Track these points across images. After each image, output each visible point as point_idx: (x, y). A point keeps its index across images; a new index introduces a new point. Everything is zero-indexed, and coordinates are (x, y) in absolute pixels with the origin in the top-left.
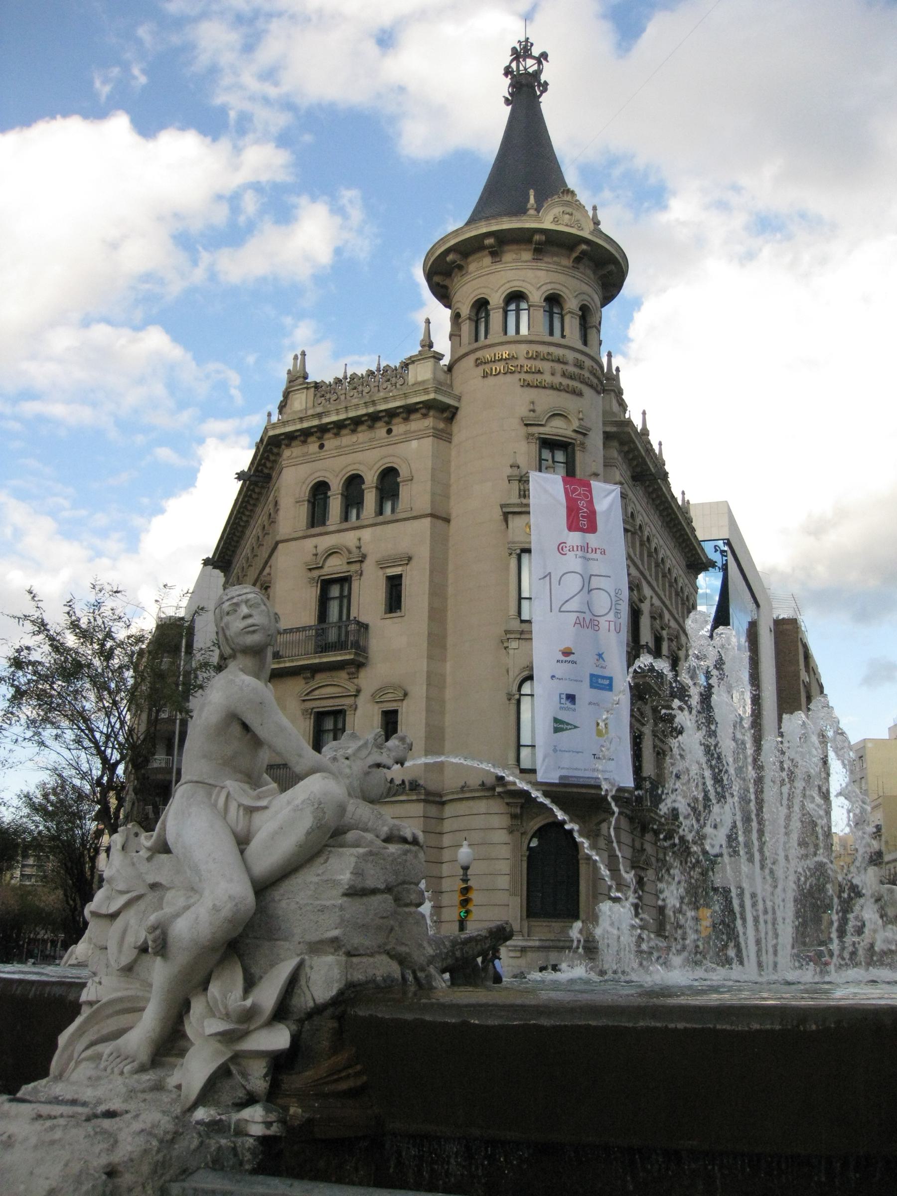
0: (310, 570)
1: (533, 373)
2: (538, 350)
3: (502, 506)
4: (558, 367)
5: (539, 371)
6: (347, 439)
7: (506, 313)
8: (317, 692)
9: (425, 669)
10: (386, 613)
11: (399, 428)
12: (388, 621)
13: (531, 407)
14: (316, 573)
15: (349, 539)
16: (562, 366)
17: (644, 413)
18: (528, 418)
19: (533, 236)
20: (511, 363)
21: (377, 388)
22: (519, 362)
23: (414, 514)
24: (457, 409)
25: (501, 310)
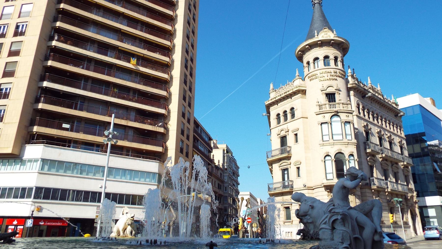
0: (278, 135)
3: (315, 113)
4: (329, 74)
7: (314, 63)
10: (295, 143)
13: (337, 85)
15: (285, 127)
17: (219, 161)
18: (322, 89)
19: (331, 41)
22: (318, 75)
24: (306, 90)
25: (313, 63)
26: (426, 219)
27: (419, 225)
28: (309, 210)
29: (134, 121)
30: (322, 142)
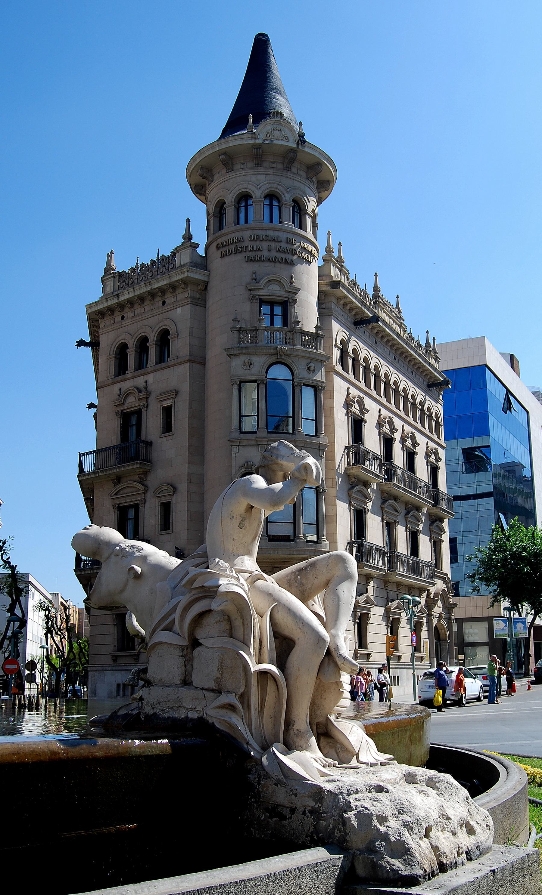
1: (255, 251)
2: (259, 234)
5: (259, 249)
6: (138, 310)
8: (121, 492)
9: (187, 472)
11: (170, 299)
12: (165, 439)
14: (120, 409)
15: (140, 382)
16: (277, 244)
20: (239, 245)
21: (157, 272)
23: (179, 360)
26: (319, 494)
27: (145, 435)
28: (126, 585)
29: (132, 538)
30: (236, 435)
